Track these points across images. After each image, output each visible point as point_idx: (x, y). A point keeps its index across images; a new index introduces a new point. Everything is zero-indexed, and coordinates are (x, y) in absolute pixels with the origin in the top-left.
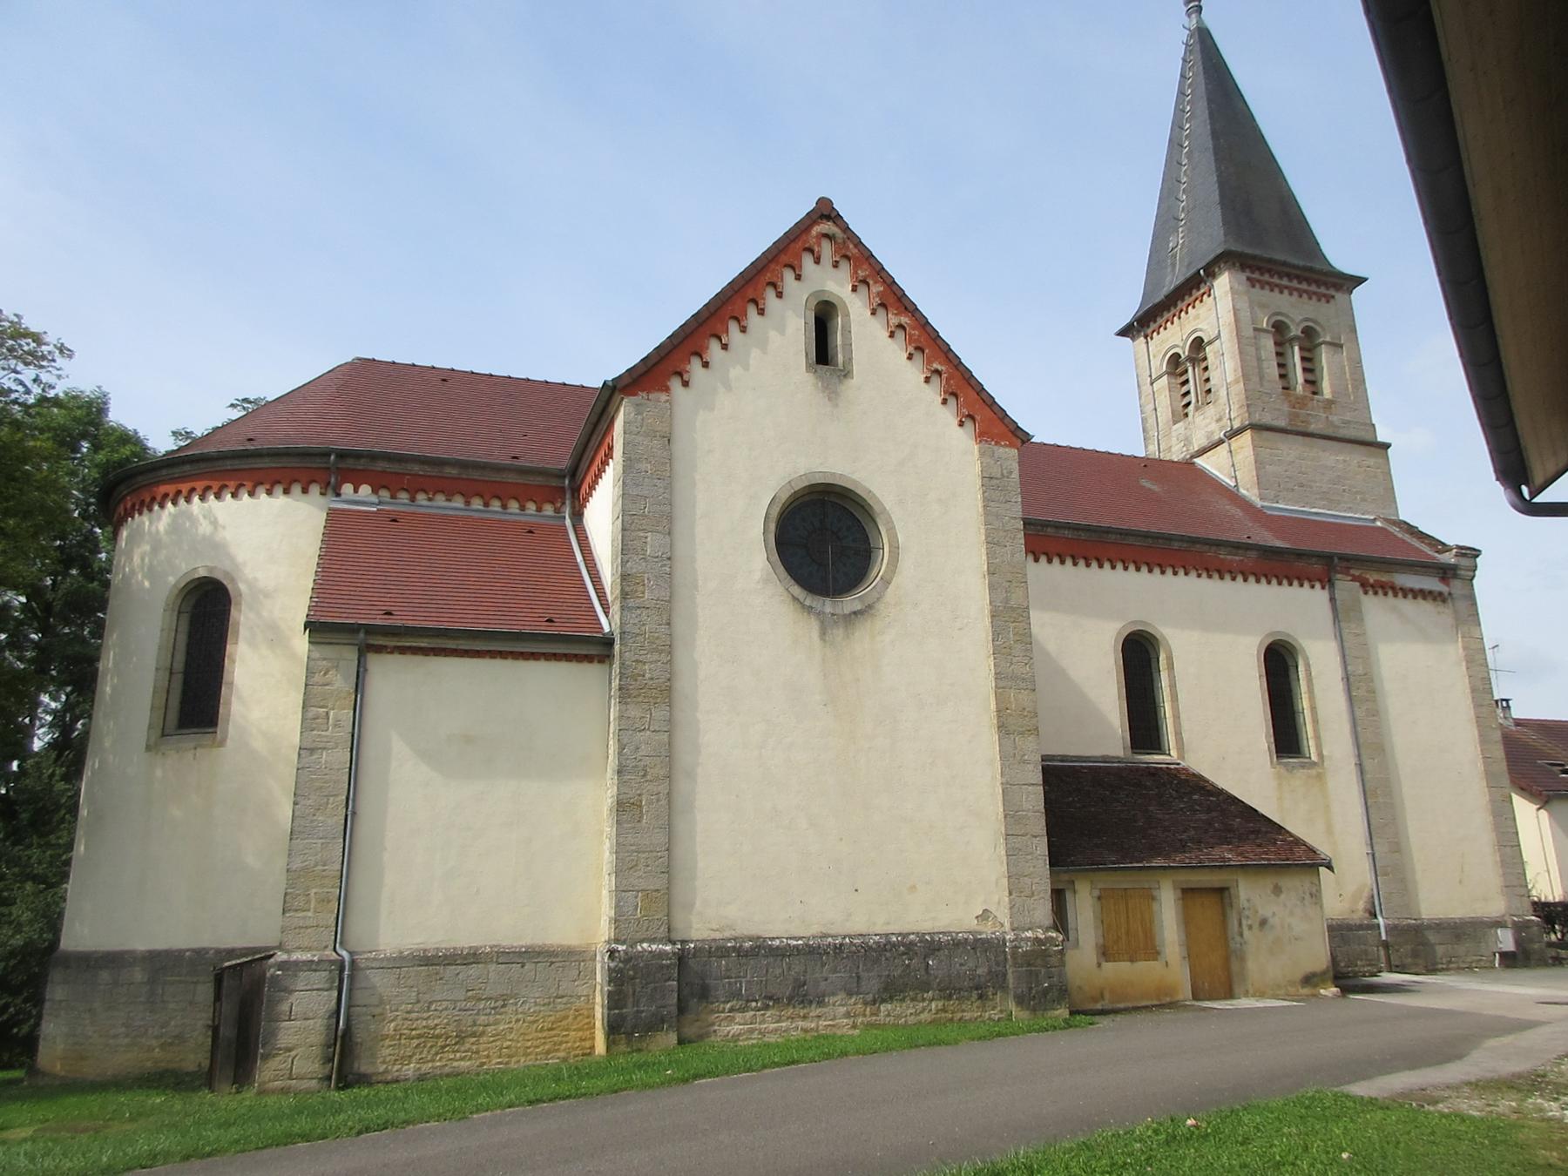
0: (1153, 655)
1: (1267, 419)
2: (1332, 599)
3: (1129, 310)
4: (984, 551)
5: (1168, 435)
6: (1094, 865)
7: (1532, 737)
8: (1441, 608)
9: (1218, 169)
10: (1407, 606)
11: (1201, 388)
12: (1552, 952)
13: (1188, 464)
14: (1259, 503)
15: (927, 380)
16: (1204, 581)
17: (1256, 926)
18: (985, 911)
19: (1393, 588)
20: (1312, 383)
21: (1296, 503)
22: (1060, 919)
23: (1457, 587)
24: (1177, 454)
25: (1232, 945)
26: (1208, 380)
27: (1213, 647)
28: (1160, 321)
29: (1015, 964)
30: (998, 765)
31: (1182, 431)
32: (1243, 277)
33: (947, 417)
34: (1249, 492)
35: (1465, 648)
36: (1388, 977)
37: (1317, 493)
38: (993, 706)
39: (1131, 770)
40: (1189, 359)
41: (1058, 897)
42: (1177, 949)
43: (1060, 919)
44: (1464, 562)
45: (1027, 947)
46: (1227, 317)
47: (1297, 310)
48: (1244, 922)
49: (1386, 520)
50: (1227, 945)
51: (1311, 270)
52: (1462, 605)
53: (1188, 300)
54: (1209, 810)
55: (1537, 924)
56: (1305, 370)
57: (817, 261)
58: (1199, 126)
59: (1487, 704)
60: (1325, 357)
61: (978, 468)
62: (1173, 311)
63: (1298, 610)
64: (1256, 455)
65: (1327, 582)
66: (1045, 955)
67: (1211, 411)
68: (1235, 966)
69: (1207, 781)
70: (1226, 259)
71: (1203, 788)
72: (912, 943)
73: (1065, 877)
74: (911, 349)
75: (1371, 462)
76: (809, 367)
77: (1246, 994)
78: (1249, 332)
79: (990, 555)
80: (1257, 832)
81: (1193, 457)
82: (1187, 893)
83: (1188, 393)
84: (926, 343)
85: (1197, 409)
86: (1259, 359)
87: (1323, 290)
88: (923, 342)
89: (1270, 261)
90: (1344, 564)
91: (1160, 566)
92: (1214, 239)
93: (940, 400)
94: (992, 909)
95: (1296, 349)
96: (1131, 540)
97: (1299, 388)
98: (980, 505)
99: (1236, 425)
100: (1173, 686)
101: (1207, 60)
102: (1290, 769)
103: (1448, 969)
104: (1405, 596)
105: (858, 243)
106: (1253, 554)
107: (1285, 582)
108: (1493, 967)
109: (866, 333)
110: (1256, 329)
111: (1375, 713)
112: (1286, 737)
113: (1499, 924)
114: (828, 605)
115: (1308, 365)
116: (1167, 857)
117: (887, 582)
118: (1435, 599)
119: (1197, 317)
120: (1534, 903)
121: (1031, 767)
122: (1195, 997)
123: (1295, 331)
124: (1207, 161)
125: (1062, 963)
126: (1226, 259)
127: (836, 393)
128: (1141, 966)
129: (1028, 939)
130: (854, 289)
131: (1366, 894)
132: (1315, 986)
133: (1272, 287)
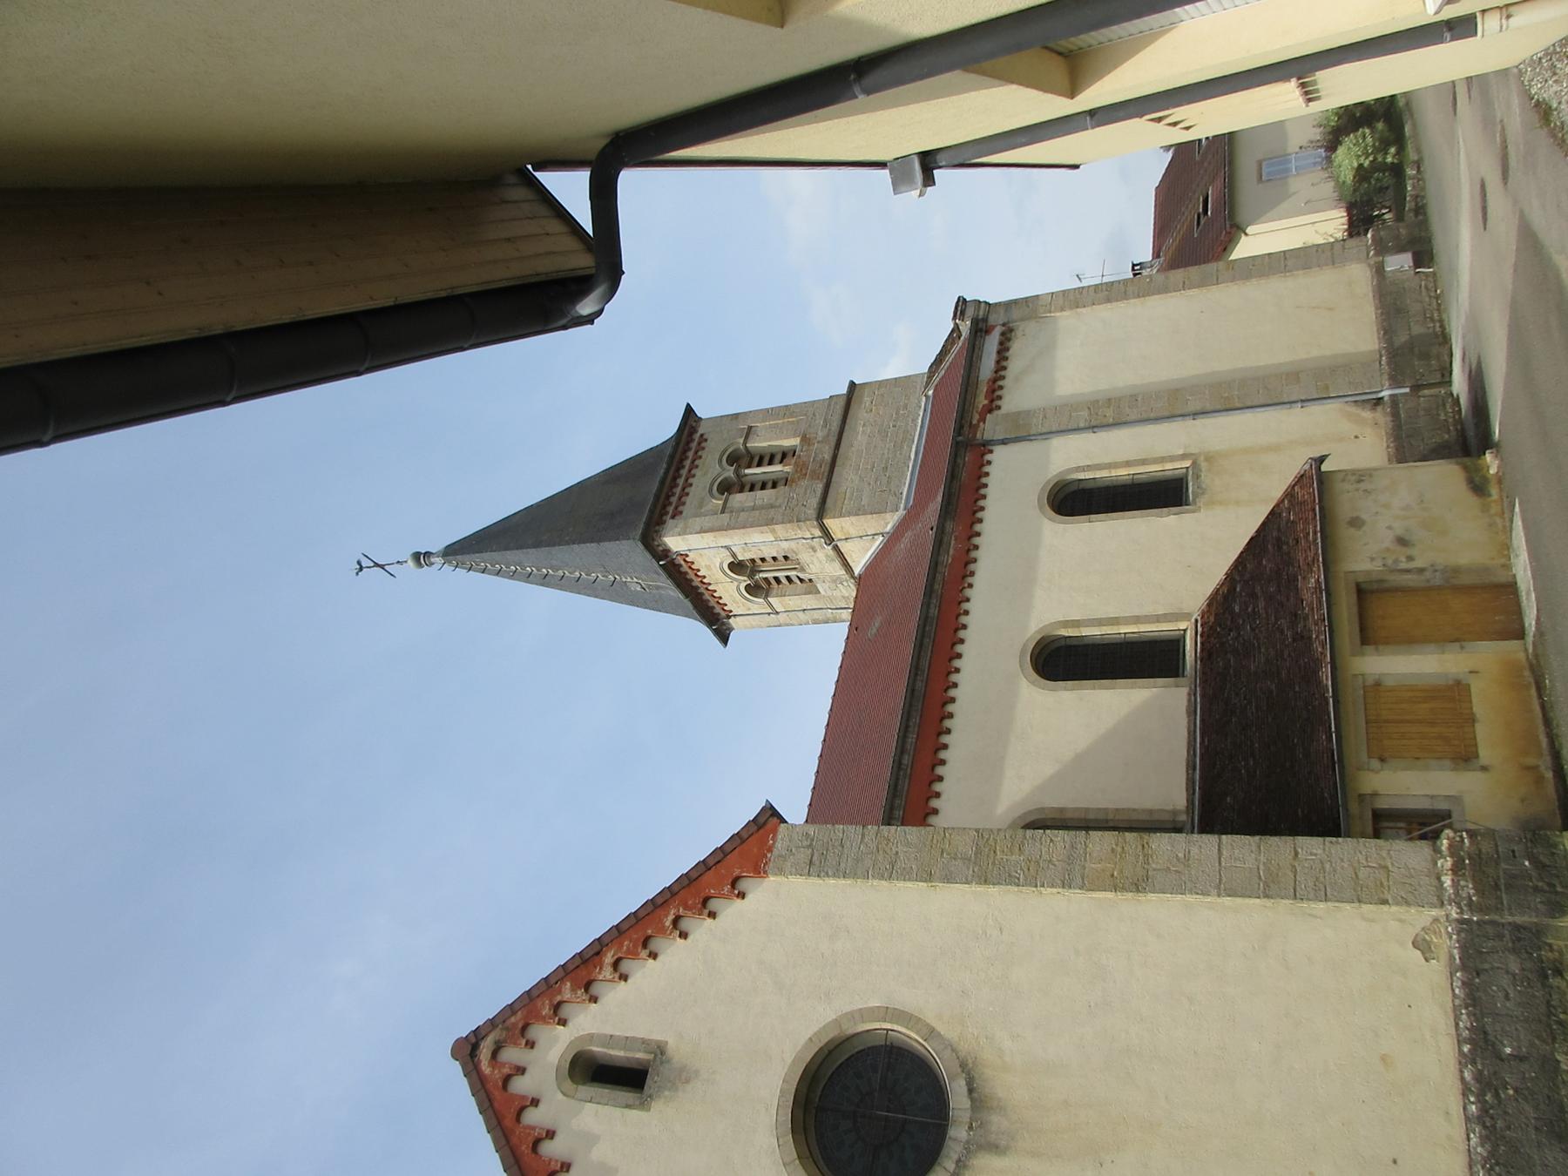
0: (1063, 643)
1: (814, 502)
2: (1004, 442)
3: (701, 632)
4: (901, 884)
5: (830, 599)
6: (1334, 765)
7: (1171, 242)
8: (1019, 333)
9: (567, 543)
10: (1014, 366)
11: (782, 564)
12: (1410, 217)
13: (860, 581)
14: (901, 512)
15: (684, 935)
16: (975, 580)
17: (1410, 552)
18: (1415, 945)
19: (995, 381)
20: (784, 455)
21: (903, 474)
22: (1424, 824)
23: (996, 319)
24: (849, 591)
25: (1438, 581)
26: (774, 559)
27: (1048, 574)
28: (712, 602)
29: (1498, 909)
30: (1190, 898)
31: (826, 586)
32: (670, 523)
33: (731, 912)
34: (890, 521)
35: (1062, 310)
36: (1459, 384)
37: (896, 455)
38: (1110, 895)
39: (1204, 682)
40: (751, 576)
41: (1385, 822)
42: (1447, 656)
43: (1424, 824)
44: (970, 312)
45: (1469, 889)
46: (707, 540)
47: (711, 468)
48: (1403, 566)
49: (928, 384)
50: (1439, 588)
51: (672, 457)
52: (1016, 314)
53: (691, 575)
54: (1253, 595)
55: (1377, 231)
56: (770, 463)
57: (521, 1070)
58: (529, 558)
59: (1137, 283)
60: (759, 444)
61: (800, 880)
62: (702, 590)
63: (1014, 479)
64: (850, 514)
65: (986, 447)
66: (1478, 860)
67: (804, 557)
68: (1466, 580)
69: (1216, 592)
70: (650, 541)
71: (1225, 597)
72: (1479, 1077)
73: (1354, 807)
74: (644, 953)
75: (867, 399)
76: (643, 1105)
77: (1507, 567)
78: (726, 516)
79: (906, 875)
80: (1279, 543)
81: (853, 576)
82: (1367, 637)
83: (788, 578)
84: (639, 933)
85: (803, 570)
86: (753, 508)
87: (694, 445)
88: (638, 935)
89: (657, 497)
90: (966, 429)
91: (956, 630)
92: (630, 551)
93: (709, 921)
94: (1410, 933)
95: (747, 471)
96: (925, 663)
97: (787, 469)
98: (842, 882)
99: (818, 533)
100: (1100, 622)
101: (465, 550)
102: (1201, 491)
103: (1441, 321)
104: (1005, 368)
105: (511, 1009)
106: (949, 526)
107: (983, 491)
108: (1434, 274)
109: (614, 1017)
110: (723, 512)
111: (1134, 398)
112: (1163, 494)
113: (1379, 270)
114: (958, 1133)
115: (766, 460)
116: (1318, 663)
117: (931, 1033)
118: (1009, 340)
119: (708, 567)
120: (1351, 235)
121: (1195, 851)
122: (1520, 634)
123: (730, 472)
124: (561, 553)
125: (1491, 834)
126: (650, 541)
127: (683, 1069)
128: (1478, 708)
129: (1455, 884)
130: (563, 1022)
131: (1353, 409)
132: (1485, 480)
133: (684, 494)
